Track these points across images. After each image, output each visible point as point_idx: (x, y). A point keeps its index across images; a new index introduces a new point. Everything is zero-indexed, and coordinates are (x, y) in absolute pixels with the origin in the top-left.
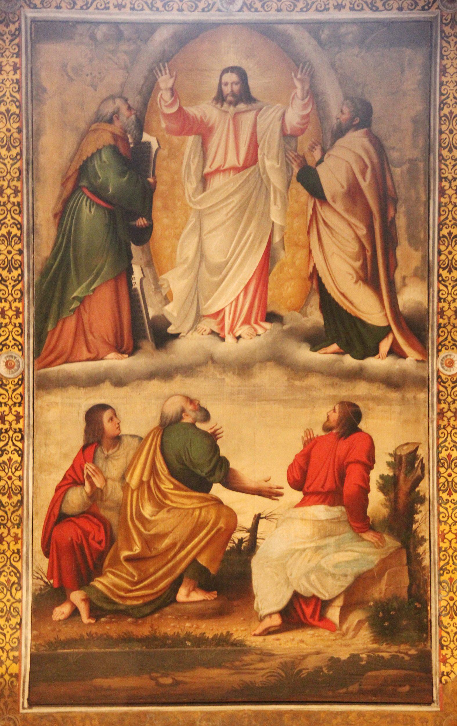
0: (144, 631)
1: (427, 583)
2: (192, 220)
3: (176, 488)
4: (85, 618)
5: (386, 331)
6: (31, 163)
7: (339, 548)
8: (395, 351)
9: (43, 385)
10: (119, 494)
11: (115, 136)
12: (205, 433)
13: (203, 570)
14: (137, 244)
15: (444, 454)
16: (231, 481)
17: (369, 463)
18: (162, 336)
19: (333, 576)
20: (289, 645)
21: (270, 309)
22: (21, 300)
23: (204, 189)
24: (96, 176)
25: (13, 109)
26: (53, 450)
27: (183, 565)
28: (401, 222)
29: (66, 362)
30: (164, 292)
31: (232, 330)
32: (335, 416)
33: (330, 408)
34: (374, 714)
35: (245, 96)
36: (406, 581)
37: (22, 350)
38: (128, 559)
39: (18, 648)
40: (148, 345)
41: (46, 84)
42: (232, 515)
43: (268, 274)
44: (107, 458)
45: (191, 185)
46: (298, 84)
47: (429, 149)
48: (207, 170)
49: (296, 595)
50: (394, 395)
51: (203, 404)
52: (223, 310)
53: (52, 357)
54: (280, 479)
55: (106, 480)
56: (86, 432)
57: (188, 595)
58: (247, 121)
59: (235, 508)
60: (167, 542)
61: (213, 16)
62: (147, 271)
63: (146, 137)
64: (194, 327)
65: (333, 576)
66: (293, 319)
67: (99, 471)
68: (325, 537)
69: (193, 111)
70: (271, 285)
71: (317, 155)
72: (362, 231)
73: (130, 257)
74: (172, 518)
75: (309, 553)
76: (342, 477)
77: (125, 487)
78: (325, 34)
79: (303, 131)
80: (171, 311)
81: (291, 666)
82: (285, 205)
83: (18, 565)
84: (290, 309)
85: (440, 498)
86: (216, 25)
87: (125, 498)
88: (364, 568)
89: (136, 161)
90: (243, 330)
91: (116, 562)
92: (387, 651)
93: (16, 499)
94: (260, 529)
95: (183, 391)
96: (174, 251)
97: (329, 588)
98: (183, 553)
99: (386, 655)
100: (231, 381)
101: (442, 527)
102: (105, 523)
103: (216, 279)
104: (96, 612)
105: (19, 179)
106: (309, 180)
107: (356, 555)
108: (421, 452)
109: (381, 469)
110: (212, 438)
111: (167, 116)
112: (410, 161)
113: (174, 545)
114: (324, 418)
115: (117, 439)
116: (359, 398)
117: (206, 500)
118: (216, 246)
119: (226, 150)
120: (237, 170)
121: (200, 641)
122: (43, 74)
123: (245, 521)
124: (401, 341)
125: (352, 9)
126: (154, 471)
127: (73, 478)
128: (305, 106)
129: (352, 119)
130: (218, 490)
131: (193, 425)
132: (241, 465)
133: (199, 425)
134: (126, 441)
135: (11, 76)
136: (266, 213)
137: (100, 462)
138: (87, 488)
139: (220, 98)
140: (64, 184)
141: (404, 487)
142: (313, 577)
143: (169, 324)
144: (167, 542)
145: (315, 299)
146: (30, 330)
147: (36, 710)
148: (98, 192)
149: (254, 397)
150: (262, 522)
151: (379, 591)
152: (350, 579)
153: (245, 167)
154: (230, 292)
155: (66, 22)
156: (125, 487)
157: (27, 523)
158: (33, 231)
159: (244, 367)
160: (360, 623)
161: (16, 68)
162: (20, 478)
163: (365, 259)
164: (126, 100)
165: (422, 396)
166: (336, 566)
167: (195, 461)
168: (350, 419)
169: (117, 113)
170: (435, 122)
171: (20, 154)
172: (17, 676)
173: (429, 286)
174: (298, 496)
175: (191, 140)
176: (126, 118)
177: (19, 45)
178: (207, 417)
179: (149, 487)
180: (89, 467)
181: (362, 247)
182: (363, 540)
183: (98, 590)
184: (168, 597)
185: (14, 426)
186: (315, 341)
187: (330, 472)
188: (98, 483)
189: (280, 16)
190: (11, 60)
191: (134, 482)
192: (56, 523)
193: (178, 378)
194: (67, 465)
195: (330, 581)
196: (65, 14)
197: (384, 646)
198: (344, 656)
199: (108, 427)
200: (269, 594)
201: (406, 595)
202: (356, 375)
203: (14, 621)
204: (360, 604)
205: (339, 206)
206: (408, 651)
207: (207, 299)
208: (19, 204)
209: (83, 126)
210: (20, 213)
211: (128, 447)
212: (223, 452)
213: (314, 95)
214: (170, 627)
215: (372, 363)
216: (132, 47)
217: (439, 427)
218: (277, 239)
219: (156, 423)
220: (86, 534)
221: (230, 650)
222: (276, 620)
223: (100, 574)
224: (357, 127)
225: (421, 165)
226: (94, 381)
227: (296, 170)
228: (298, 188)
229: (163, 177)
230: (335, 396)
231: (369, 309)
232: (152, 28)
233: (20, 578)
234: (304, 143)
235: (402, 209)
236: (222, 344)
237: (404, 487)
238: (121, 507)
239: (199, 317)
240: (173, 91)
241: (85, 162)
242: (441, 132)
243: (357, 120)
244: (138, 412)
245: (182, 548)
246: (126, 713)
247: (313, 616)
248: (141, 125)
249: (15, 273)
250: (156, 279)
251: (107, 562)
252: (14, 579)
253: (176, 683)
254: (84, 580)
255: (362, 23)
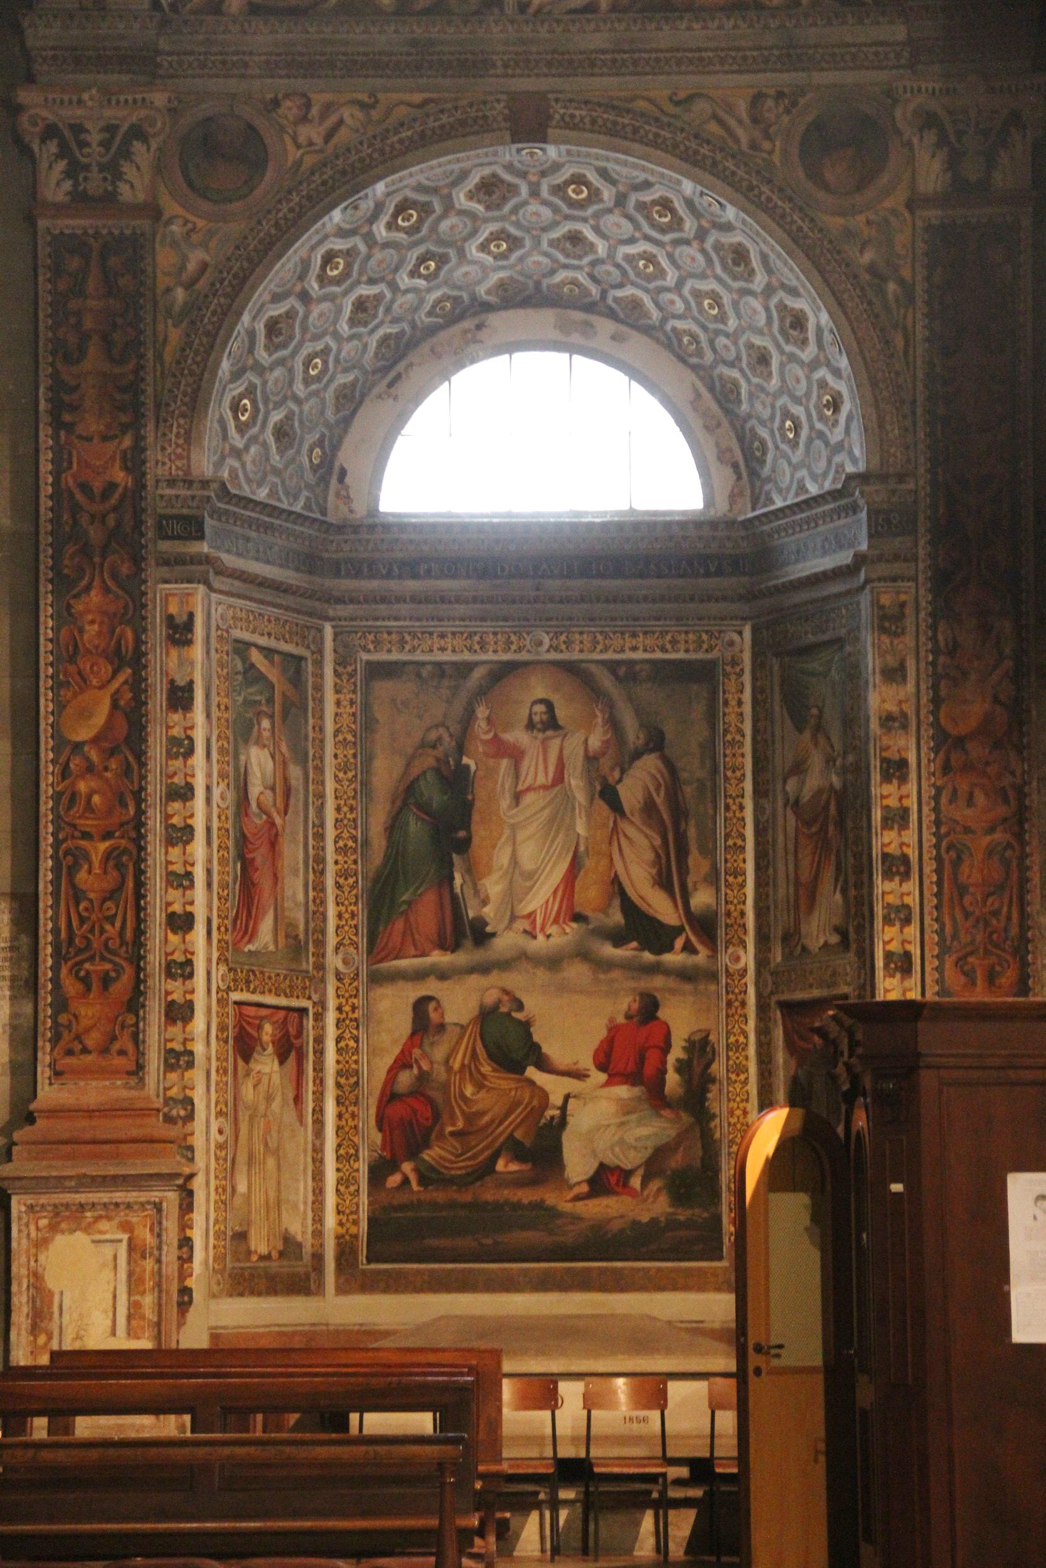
0: (468, 1197)
1: (717, 1155)
2: (507, 832)
3: (494, 1070)
4: (415, 1186)
5: (680, 930)
6: (366, 784)
7: (640, 1123)
8: (688, 948)
9: (376, 979)
10: (443, 1076)
11: (438, 760)
12: (520, 1022)
13: (518, 1143)
14: (458, 853)
15: (732, 1039)
16: (543, 1064)
17: (667, 1047)
18: (481, 935)
19: (635, 1148)
20: (597, 1210)
21: (577, 909)
22: (356, 904)
23: (517, 804)
24: (422, 795)
25: (350, 738)
26: (384, 1036)
27: (501, 1139)
28: (692, 833)
29: (397, 958)
30: (482, 896)
31: (542, 929)
32: (636, 1006)
33: (631, 998)
34: (672, 1270)
35: (552, 723)
36: (700, 1153)
37: (357, 948)
38: (452, 1134)
39: (357, 1212)
40: (468, 943)
41: (378, 716)
42: (544, 1096)
43: (575, 877)
44: (432, 1044)
45: (505, 802)
46: (599, 714)
47: (715, 770)
48: (520, 788)
49: (602, 1165)
50: (688, 987)
51: (518, 994)
52: (534, 912)
53: (383, 954)
54: (586, 1062)
55: (432, 1063)
56: (414, 1022)
57: (506, 1166)
58: (554, 745)
59: (548, 1088)
60: (487, 1118)
61: (524, 656)
62: (467, 877)
63: (465, 760)
64: (509, 927)
65: (635, 1148)
66: (597, 919)
67: (425, 1055)
68: (628, 1113)
69: (509, 737)
70: (577, 889)
71: (617, 774)
72: (658, 842)
73: (451, 864)
74: (488, 1096)
75: (613, 1129)
76: (642, 1060)
77: (449, 1069)
78: (622, 671)
79: (604, 754)
80: (488, 911)
81: (599, 1227)
82: (589, 816)
83: (356, 1139)
84: (594, 910)
85: (729, 1078)
86: (526, 664)
87: (448, 1080)
88: (665, 1140)
89: (457, 782)
90: (552, 930)
91: (441, 1136)
92: (683, 1215)
93: (353, 1080)
94: (569, 1107)
95: (500, 984)
96: (491, 859)
97: (631, 1159)
98: (501, 1129)
99: (682, 1218)
100: (542, 975)
101: (732, 1104)
102: (431, 1101)
103: (528, 884)
104: (423, 1180)
105: (354, 798)
106: (609, 796)
107: (651, 1131)
108: (712, 1038)
109: (676, 1053)
110: (526, 1026)
111: (485, 742)
112: (698, 780)
113: (493, 1121)
114: (625, 1006)
115: (442, 1027)
116: (656, 989)
117: (519, 1081)
118: (528, 854)
119: (536, 771)
120: (545, 788)
121: (518, 1206)
122: (376, 707)
123: (556, 1099)
124: (693, 939)
125: (645, 650)
126: (474, 1056)
127: (402, 1063)
128: (605, 733)
129: (647, 744)
130: (531, 1072)
131: (508, 1014)
132: (552, 1049)
133: (514, 1014)
134: (449, 1028)
135: (350, 1122)
136: (572, 827)
137: (427, 1048)
138: (415, 1071)
139: (530, 725)
140: (393, 802)
141: (697, 1069)
142: (617, 1149)
143: (487, 924)
144: (487, 1118)
145: (617, 902)
146: (363, 930)
147: (373, 1266)
148: (424, 808)
149: (563, 988)
150: (571, 1101)
151: (676, 1161)
152: (650, 1151)
153: (553, 785)
154: (540, 898)
155: (396, 663)
156: (449, 1069)
157: (363, 1102)
158: (366, 842)
159: (553, 962)
160: (659, 1190)
161: (352, 702)
162: (356, 1062)
163: (660, 864)
164: (448, 728)
165: (713, 987)
166: (638, 1139)
167: (509, 1044)
168: (649, 1008)
169: (439, 739)
170: (720, 748)
171: (355, 776)
172: (356, 1237)
173: (718, 890)
174: (603, 1077)
175: (505, 763)
176: (448, 743)
177: (355, 684)
178: (520, 1006)
179: (470, 1070)
180: (416, 1052)
181: (658, 855)
182: (661, 1116)
183: (424, 1161)
184: (489, 1167)
185: (351, 1015)
186: (618, 938)
187: (629, 1055)
188: (425, 1066)
189: (583, 656)
190: (351, 1109)
191: (457, 1066)
192: (389, 1101)
193: (495, 972)
194: (397, 1050)
195: (632, 1154)
196: (395, 656)
197: (680, 1210)
198: (645, 1218)
199: (433, 1016)
200: (578, 1164)
201: (699, 1165)
202: (654, 969)
203: (352, 1188)
204: (660, 1173)
205: (636, 819)
206: (699, 1214)
207: (521, 901)
208: (354, 820)
209: (410, 751)
210: (355, 828)
211: (451, 1034)
212: (536, 1038)
213: (614, 724)
214: (490, 1195)
215: (668, 958)
216: (453, 683)
217: (727, 1016)
218: (582, 848)
219: (476, 1013)
220: (415, 1112)
221: (545, 1214)
222: (585, 1188)
223: (427, 1145)
224: (651, 751)
225: (708, 784)
226: (420, 976)
227: (598, 788)
228: (600, 804)
229: (480, 794)
230: (634, 989)
231: (663, 908)
232: (470, 667)
233: (357, 1151)
234: (605, 763)
235: (692, 822)
236: (534, 942)
237: (697, 1069)
238: (446, 1086)
239: (513, 918)
240: (489, 720)
241: (412, 783)
242: (725, 756)
243: (652, 745)
244: (459, 1003)
245: (500, 1123)
246: (452, 1270)
247: (617, 1184)
248: (461, 750)
249: (351, 881)
250: (475, 886)
251: (433, 1136)
252: (352, 1151)
253: (496, 1243)
254: (413, 1154)
255: (653, 662)
